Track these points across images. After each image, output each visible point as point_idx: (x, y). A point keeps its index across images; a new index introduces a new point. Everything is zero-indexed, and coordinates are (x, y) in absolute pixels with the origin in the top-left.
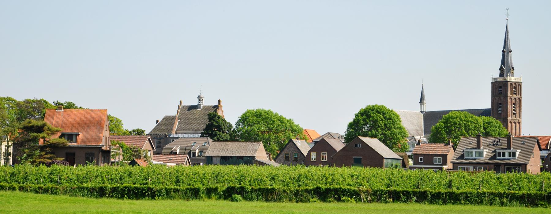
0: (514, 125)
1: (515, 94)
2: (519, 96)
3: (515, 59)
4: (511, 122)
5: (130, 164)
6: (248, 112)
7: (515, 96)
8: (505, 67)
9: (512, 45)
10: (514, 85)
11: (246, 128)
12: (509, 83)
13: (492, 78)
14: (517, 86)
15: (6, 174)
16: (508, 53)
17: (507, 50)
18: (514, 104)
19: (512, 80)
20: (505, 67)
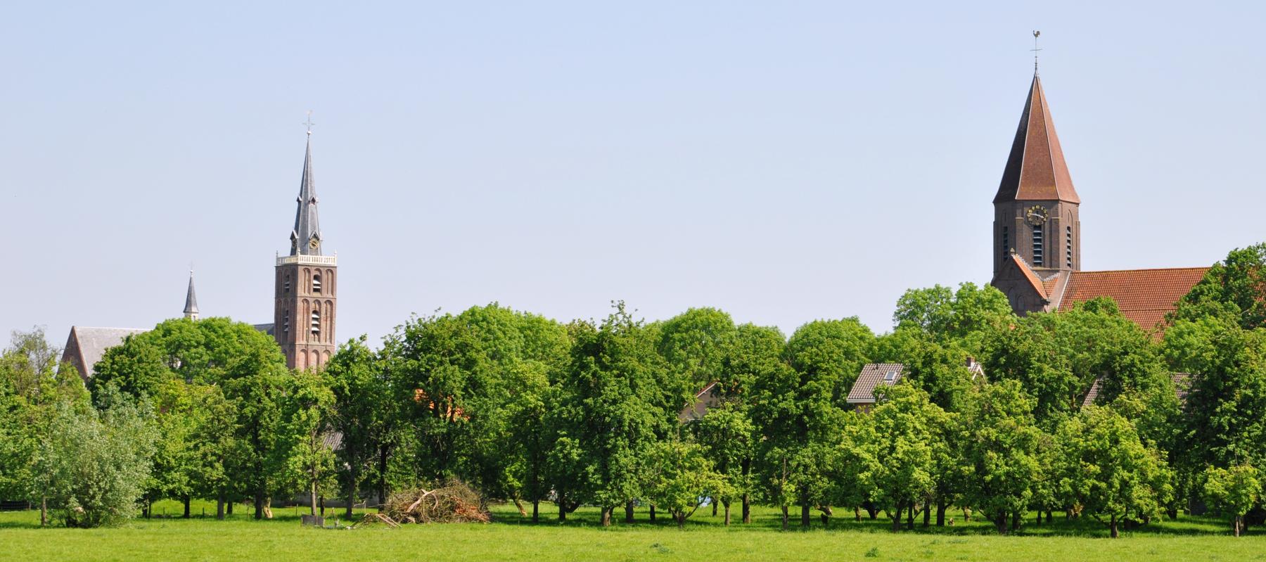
0: (313, 357)
1: (315, 290)
2: (330, 296)
3: (323, 219)
4: (305, 351)
5: (304, 463)
6: (813, 326)
7: (317, 295)
8: (303, 238)
9: (318, 189)
10: (314, 273)
11: (1085, 328)
12: (300, 269)
13: (278, 259)
14: (323, 275)
15: (847, 407)
16: (306, 205)
17: (306, 198)
18: (315, 312)
19: (311, 262)
20: (303, 238)
